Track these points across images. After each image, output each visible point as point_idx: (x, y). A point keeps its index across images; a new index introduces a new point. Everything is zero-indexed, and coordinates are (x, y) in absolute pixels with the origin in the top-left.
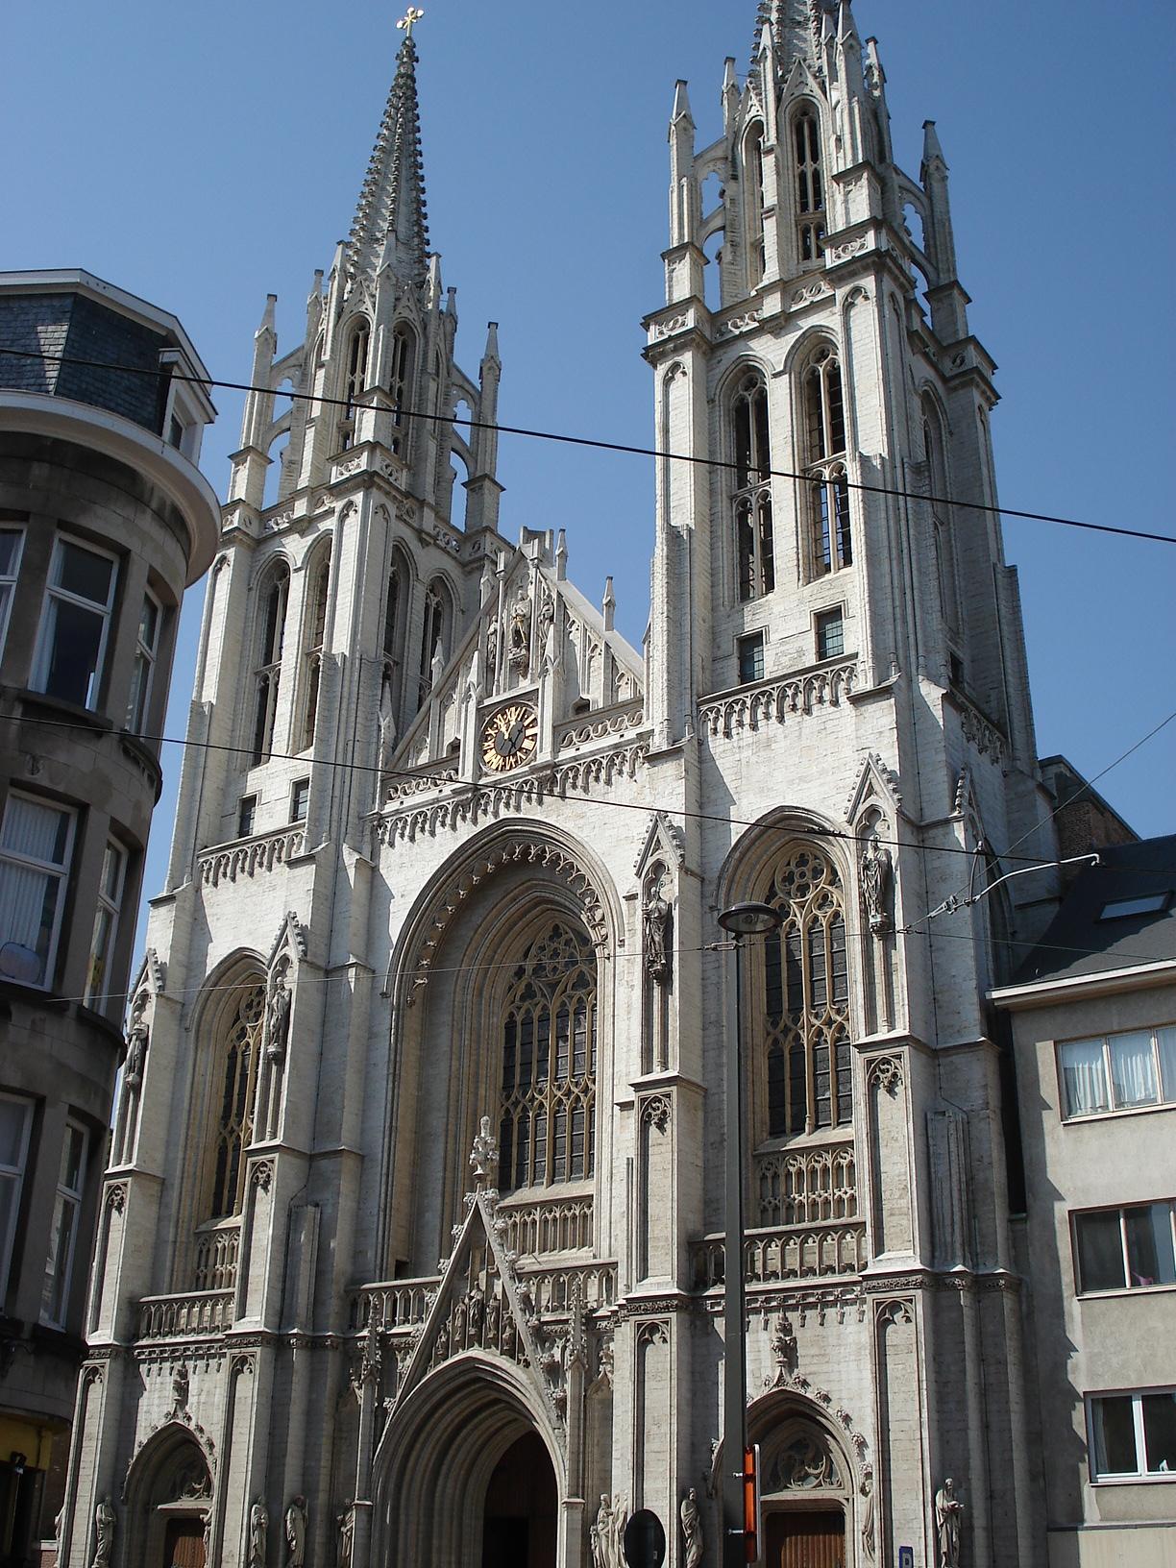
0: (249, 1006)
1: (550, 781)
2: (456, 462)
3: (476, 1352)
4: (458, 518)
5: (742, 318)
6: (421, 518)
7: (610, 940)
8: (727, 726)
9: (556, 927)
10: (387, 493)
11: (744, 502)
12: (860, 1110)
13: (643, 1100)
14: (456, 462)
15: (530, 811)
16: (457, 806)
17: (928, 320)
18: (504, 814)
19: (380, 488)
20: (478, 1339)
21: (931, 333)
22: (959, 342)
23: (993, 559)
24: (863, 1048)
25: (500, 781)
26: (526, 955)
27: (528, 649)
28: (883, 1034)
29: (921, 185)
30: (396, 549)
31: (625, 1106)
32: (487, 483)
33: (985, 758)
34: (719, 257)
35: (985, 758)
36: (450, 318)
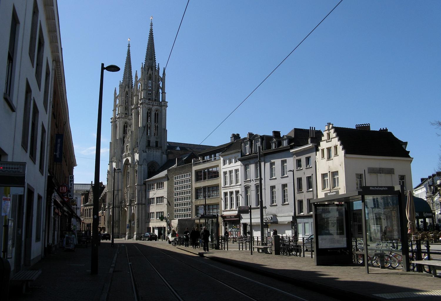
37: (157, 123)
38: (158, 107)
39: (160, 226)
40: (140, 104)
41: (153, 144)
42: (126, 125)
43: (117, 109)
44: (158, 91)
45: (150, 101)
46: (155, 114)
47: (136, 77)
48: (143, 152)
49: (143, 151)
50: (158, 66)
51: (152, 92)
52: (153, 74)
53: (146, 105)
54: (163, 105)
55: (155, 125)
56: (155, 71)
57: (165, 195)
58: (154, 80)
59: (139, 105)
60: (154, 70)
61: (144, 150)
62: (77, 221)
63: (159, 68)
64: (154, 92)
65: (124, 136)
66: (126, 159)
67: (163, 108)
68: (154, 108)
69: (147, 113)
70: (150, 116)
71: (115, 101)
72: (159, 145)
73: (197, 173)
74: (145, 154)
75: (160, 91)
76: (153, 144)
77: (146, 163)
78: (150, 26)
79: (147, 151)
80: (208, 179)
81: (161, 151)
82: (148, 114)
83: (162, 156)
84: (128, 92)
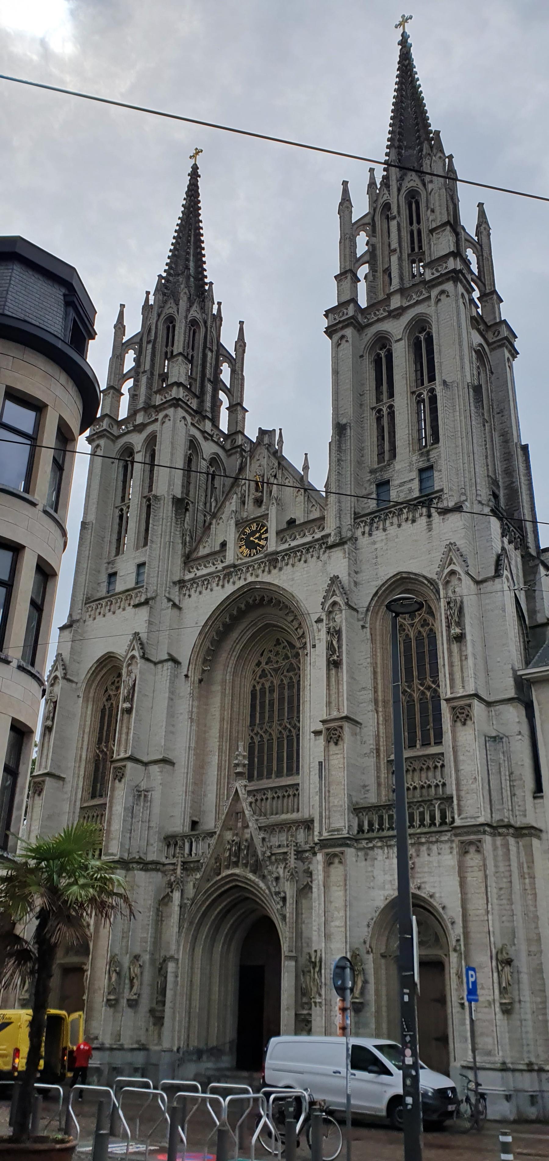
0: (113, 683)
1: (273, 561)
2: (222, 395)
3: (237, 871)
4: (224, 426)
5: (378, 310)
6: (204, 426)
7: (308, 645)
8: (370, 530)
9: (278, 640)
10: (186, 411)
11: (380, 411)
12: (448, 737)
13: (328, 729)
14: (222, 395)
15: (265, 578)
16: (225, 575)
17: (480, 310)
18: (250, 579)
19: (182, 408)
20: (236, 864)
21: (481, 317)
22: (496, 324)
23: (515, 441)
24: (447, 700)
25: (248, 562)
26: (262, 655)
27: (262, 492)
28: (461, 693)
29: (476, 238)
30: (191, 441)
31: (317, 733)
32: (239, 408)
33: (512, 546)
34: (366, 278)
35: (512, 546)
36: (218, 319)
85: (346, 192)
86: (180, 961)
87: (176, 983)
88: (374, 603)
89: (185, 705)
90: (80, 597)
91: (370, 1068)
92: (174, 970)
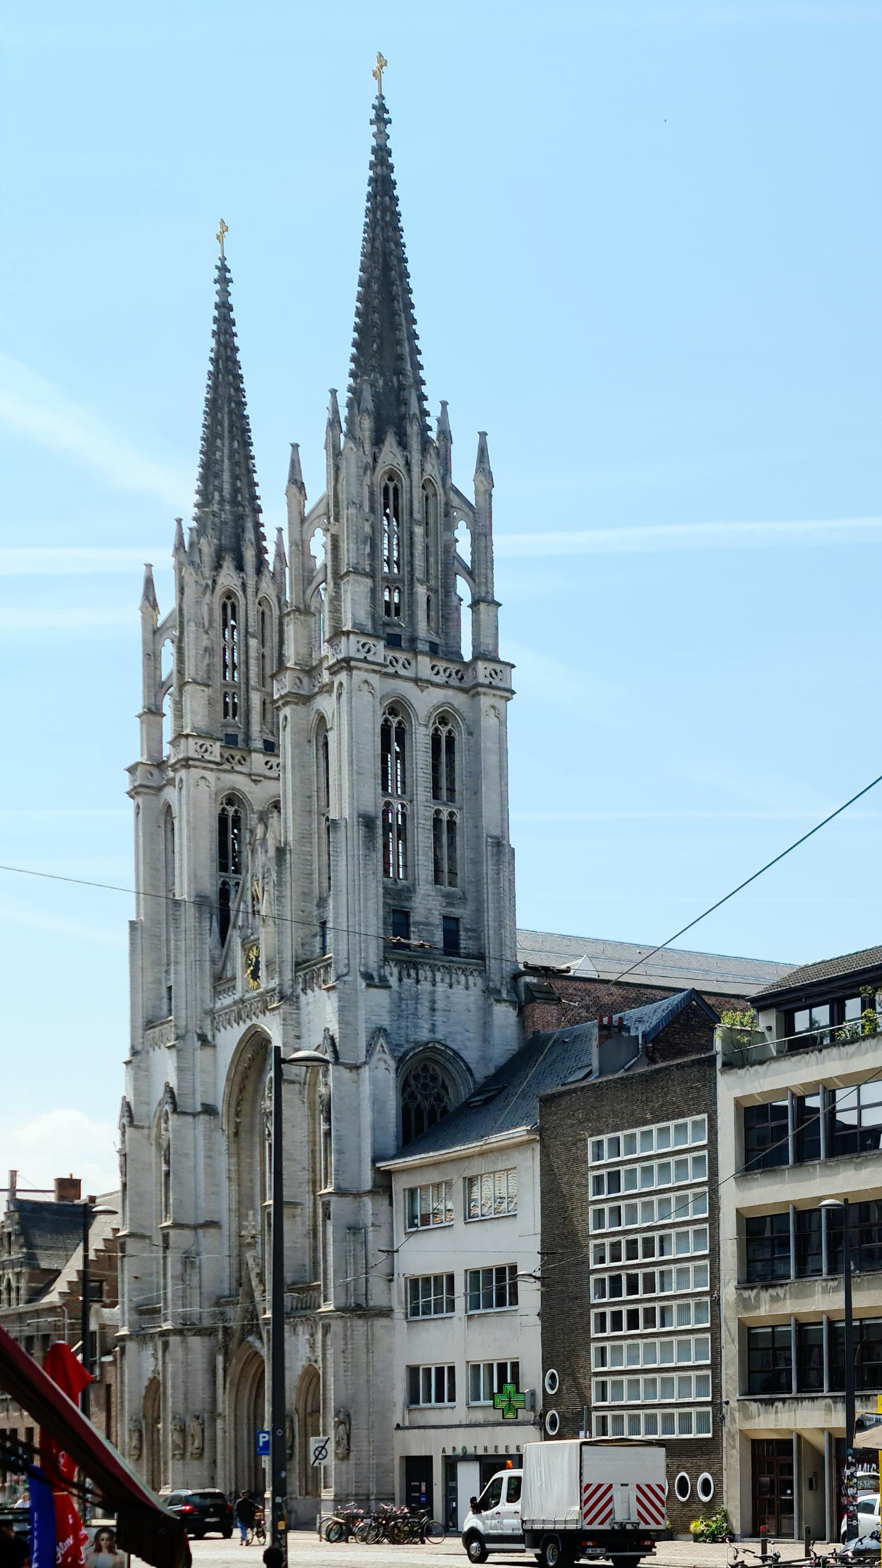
37: (451, 798)
38: (450, 692)
39: (491, 1452)
40: (334, 670)
41: (427, 932)
42: (231, 810)
43: (167, 705)
44: (448, 589)
45: (398, 655)
46: (436, 739)
47: (296, 483)
48: (369, 986)
49: (367, 976)
50: (443, 421)
51: (412, 594)
52: (409, 471)
53: (374, 679)
54: (483, 678)
55: (438, 812)
56: (424, 451)
57: (530, 1262)
58: (417, 516)
59: (326, 677)
60: (415, 444)
61: (375, 974)
62: (190, 1319)
63: (445, 435)
64: (421, 591)
65: (224, 883)
66: (243, 1027)
67: (485, 702)
68: (424, 703)
69: (378, 730)
70: (400, 756)
71: (152, 657)
72: (465, 943)
73: (757, 1119)
74: (381, 997)
75: (463, 588)
76: (427, 932)
77: (388, 1057)
78: (374, 128)
79: (393, 981)
80: (832, 1153)
81: (479, 981)
82: (393, 735)
83: (487, 1012)
84: (240, 594)
85: (149, 582)
86: (227, 1418)
87: (224, 1438)
88: (308, 1075)
89: (223, 1162)
90: (140, 1022)
91: (208, 1535)
92: (221, 1426)
